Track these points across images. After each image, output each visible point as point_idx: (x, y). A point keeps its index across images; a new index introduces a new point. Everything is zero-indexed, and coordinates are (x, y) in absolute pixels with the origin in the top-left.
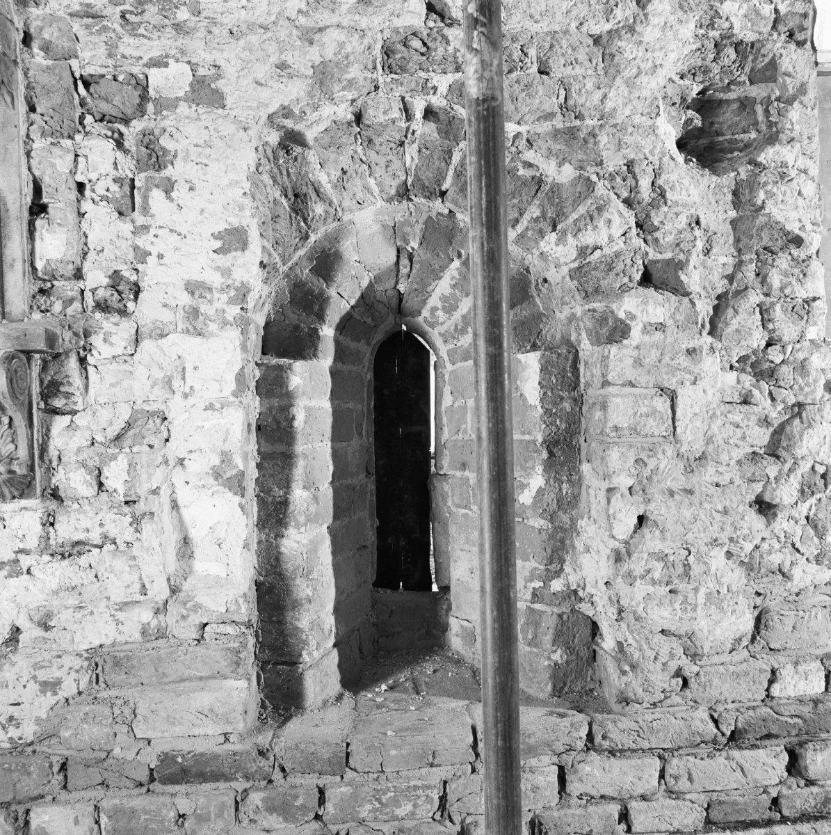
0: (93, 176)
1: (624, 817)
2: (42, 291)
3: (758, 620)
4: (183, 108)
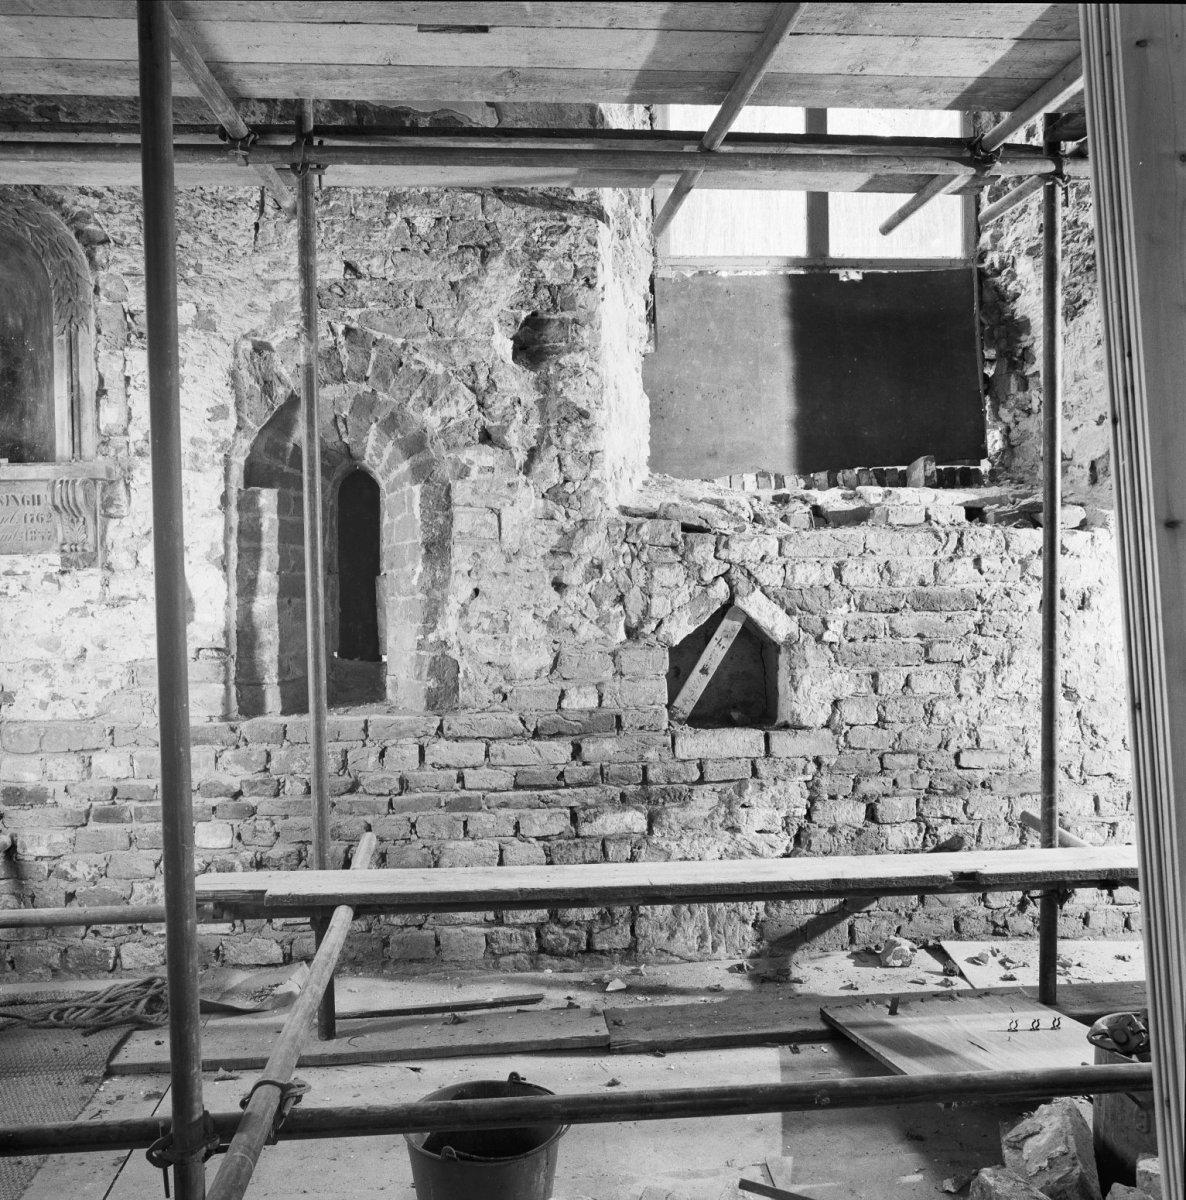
0: (136, 373)
1: (461, 779)
2: (103, 443)
3: (556, 660)
4: (190, 331)
